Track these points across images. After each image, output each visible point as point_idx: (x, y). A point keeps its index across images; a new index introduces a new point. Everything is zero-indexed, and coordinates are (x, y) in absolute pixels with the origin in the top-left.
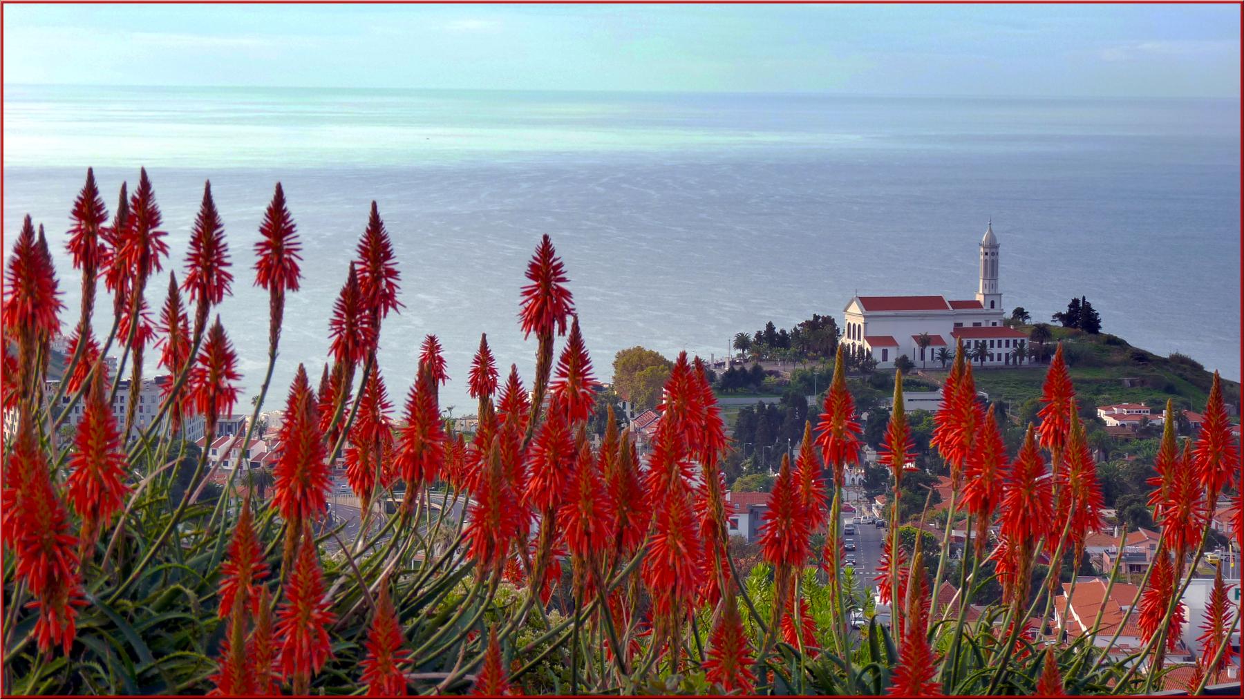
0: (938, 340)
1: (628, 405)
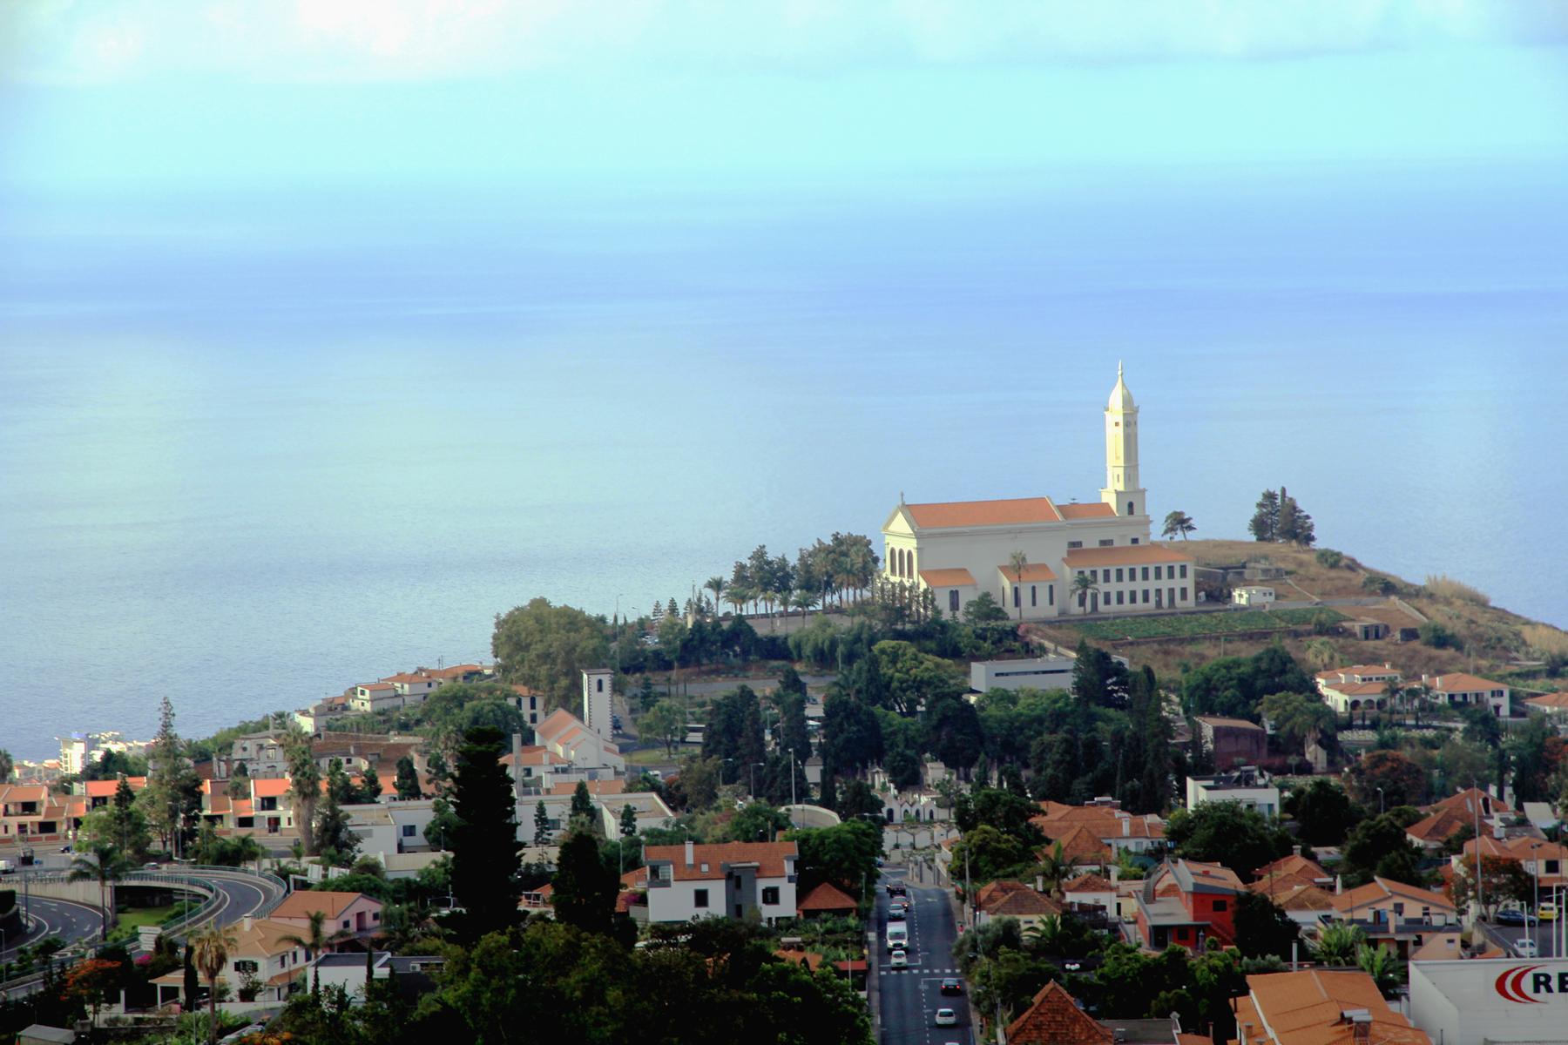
1: (526, 703)
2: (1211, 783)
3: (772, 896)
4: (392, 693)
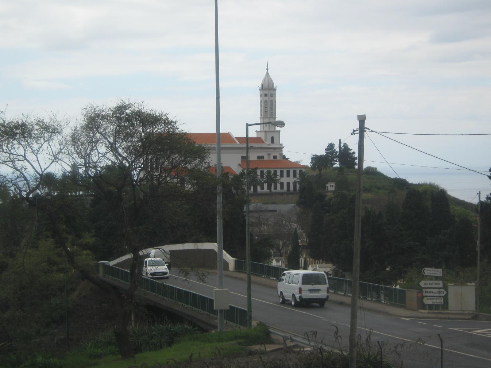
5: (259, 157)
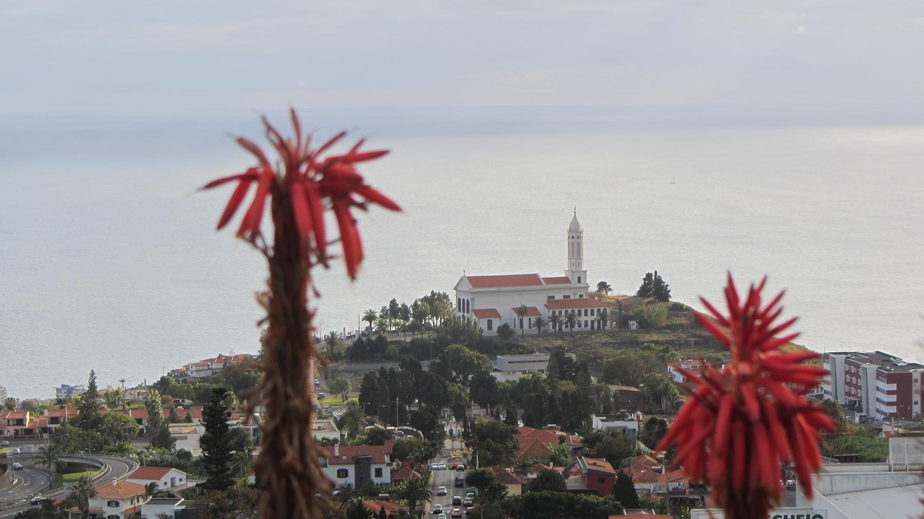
0: (534, 311)
2: (604, 418)
3: (379, 473)
4: (206, 368)
5: (565, 297)
